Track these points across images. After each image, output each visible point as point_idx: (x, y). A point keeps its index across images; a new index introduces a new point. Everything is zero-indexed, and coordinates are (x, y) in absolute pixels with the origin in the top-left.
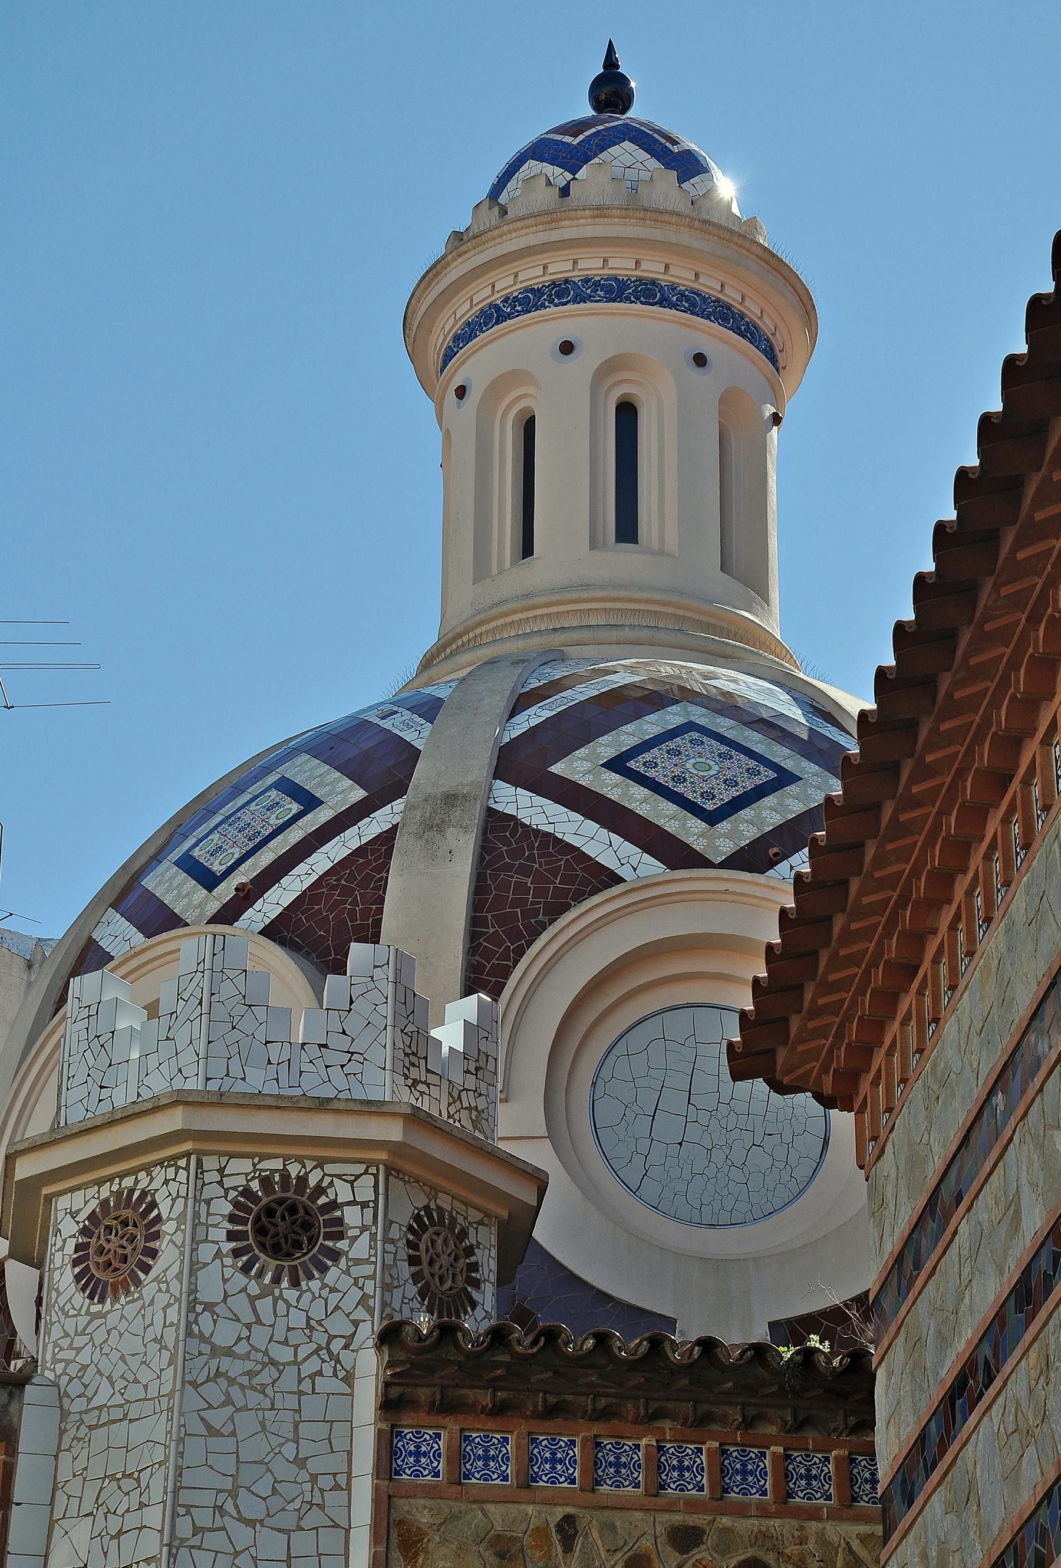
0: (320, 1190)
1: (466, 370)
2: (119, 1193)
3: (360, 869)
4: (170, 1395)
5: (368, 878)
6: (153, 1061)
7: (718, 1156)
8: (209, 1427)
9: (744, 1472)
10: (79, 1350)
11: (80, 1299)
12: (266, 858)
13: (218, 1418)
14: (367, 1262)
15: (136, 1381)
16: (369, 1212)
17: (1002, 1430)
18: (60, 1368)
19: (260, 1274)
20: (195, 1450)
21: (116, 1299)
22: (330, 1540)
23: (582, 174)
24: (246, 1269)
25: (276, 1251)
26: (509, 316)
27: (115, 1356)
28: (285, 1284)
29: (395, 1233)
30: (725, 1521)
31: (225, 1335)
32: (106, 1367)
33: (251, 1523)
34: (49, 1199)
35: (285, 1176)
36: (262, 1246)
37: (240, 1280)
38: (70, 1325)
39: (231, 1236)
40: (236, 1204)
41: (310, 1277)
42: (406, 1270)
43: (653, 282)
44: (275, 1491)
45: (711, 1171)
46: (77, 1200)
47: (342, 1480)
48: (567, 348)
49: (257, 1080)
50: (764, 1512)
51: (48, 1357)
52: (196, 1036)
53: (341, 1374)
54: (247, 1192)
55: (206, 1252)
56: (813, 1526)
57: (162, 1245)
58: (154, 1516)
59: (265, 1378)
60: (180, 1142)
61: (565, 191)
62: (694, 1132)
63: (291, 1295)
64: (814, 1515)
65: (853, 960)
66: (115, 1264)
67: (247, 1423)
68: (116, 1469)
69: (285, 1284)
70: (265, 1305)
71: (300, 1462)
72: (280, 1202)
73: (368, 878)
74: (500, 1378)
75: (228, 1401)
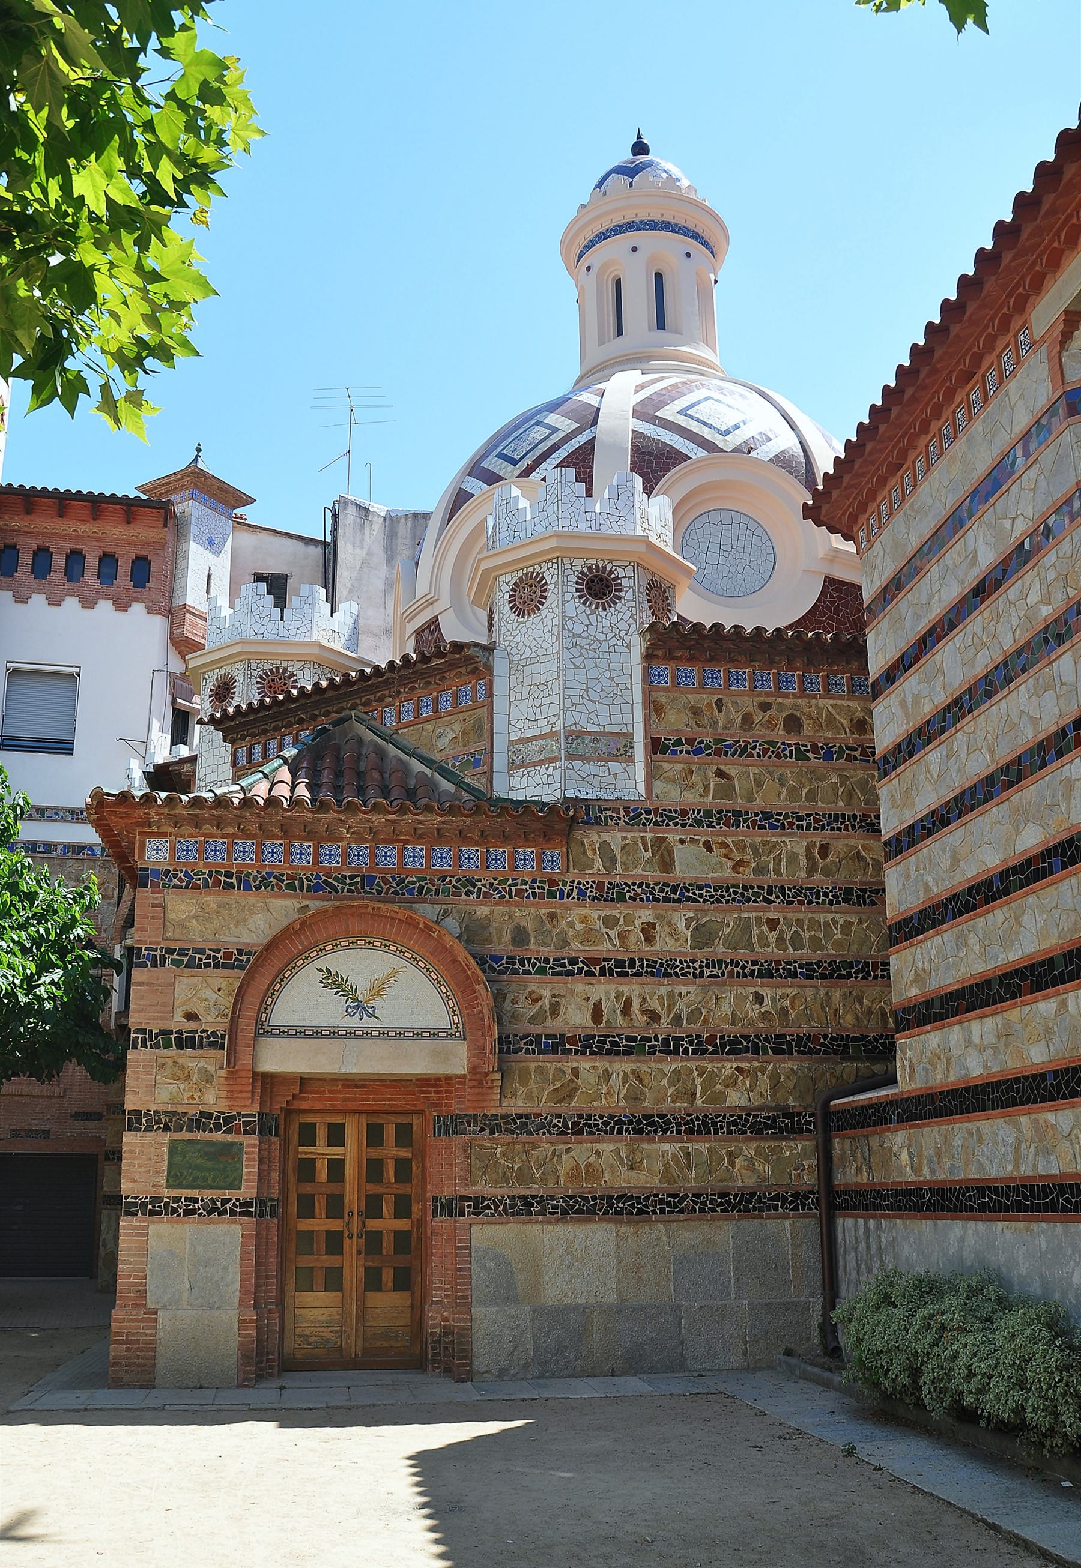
0: (611, 572)
1: (589, 259)
2: (527, 574)
3: (580, 455)
4: (558, 653)
5: (584, 458)
6: (537, 520)
7: (732, 569)
8: (574, 665)
9: (787, 682)
10: (515, 636)
11: (513, 616)
12: (538, 452)
13: (578, 661)
14: (632, 601)
15: (542, 648)
16: (632, 581)
17: (962, 645)
18: (507, 643)
19: (590, 605)
20: (570, 674)
21: (529, 616)
22: (626, 708)
23: (637, 178)
24: (584, 603)
25: (595, 596)
26: (609, 237)
27: (531, 638)
28: (600, 609)
29: (642, 590)
30: (780, 700)
31: (578, 629)
32: (527, 643)
33: (593, 701)
34: (495, 578)
35: (597, 567)
36: (590, 594)
37: (582, 607)
38: (510, 627)
39: (577, 590)
40: (578, 578)
41: (610, 607)
42: (646, 604)
43: (668, 222)
44: (602, 690)
45: (730, 575)
46: (508, 577)
47: (629, 686)
48: (634, 249)
49: (583, 527)
50: (795, 696)
51: (501, 639)
52: (556, 509)
53: (625, 645)
54: (582, 573)
55: (568, 597)
56: (814, 701)
57: (548, 594)
58: (555, 699)
59: (594, 646)
60: (239, 656)
61: (631, 184)
62: (722, 560)
63: (603, 613)
64: (814, 697)
65: (872, 463)
66: (528, 602)
67: (590, 664)
68: (536, 681)
69: (600, 609)
70: (593, 618)
71: (612, 679)
72: (596, 577)
73: (584, 458)
74: (693, 645)
75: (581, 655)
